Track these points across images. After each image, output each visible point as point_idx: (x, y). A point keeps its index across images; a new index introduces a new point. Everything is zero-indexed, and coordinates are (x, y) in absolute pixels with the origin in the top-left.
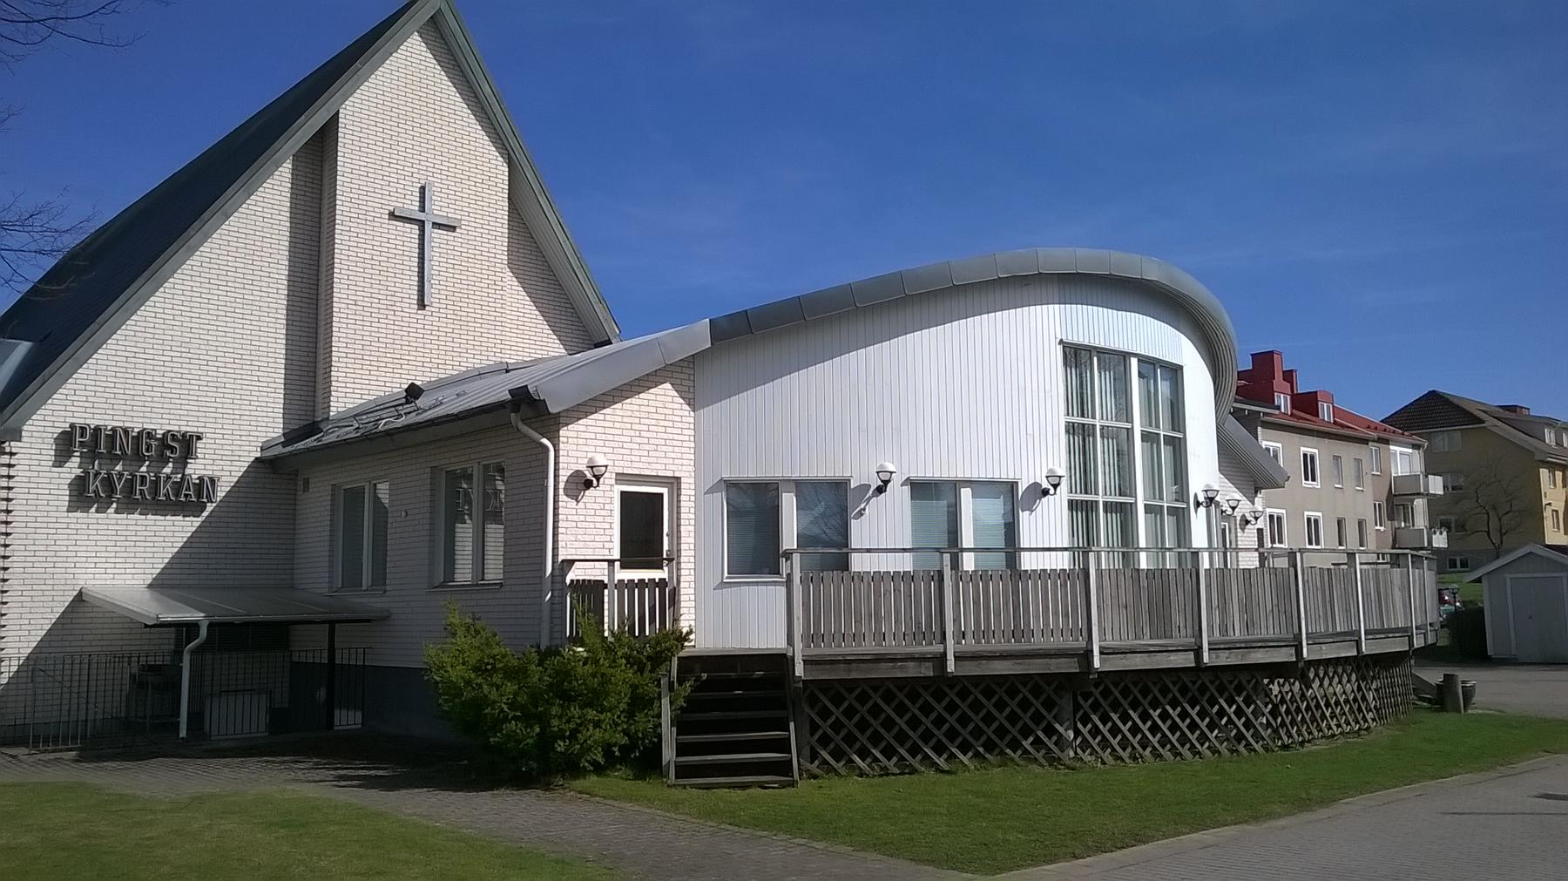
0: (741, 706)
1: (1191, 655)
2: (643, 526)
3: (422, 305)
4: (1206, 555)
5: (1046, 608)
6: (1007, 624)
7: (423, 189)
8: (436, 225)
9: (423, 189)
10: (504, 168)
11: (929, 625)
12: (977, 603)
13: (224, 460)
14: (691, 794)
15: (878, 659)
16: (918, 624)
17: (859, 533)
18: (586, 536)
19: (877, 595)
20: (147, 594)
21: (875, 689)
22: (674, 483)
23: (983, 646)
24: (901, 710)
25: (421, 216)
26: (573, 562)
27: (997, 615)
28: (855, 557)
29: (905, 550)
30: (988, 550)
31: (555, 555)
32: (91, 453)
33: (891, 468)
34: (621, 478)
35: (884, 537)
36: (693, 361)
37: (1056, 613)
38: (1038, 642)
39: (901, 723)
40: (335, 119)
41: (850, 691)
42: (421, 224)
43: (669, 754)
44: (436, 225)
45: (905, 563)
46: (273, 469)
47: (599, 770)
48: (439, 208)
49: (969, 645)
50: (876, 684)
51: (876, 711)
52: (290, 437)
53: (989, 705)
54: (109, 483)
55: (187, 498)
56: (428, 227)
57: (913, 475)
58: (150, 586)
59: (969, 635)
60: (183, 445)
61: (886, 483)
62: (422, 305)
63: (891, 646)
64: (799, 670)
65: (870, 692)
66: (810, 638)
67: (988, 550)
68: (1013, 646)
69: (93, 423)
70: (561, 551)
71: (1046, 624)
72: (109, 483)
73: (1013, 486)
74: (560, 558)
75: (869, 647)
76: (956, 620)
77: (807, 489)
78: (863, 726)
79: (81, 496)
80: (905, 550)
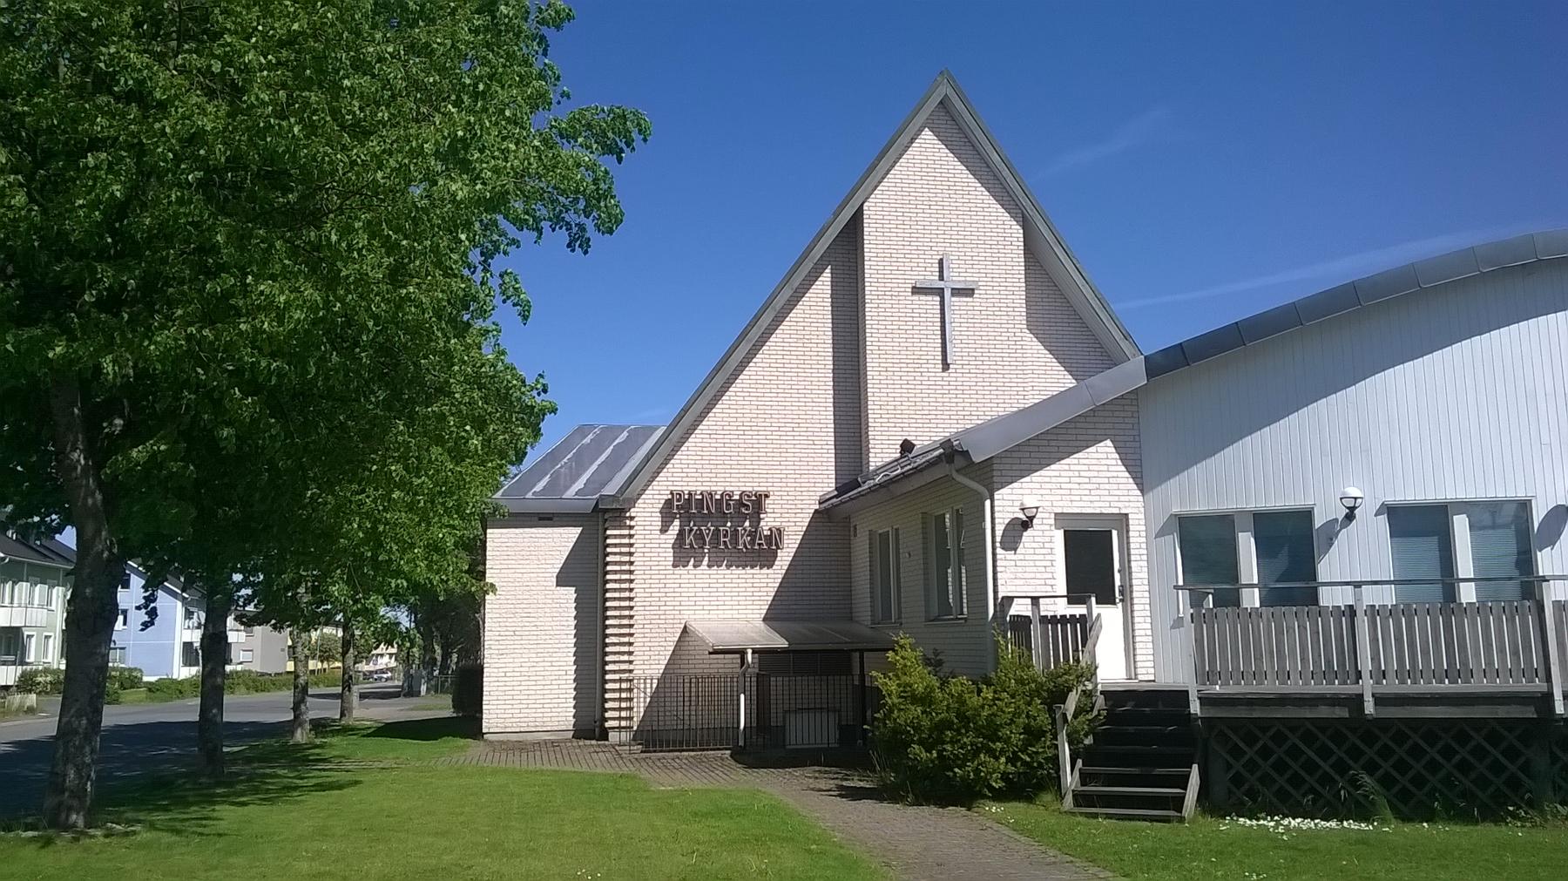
0: (1143, 744)
1: (287, 696)
2: (1091, 558)
3: (946, 366)
4: (36, 602)
5: (1488, 645)
6: (1316, 663)
7: (941, 262)
8: (957, 292)
9: (941, 262)
10: (1018, 232)
11: (1342, 663)
12: (1399, 640)
13: (790, 516)
14: (1102, 828)
15: (1283, 700)
16: (1329, 662)
17: (1326, 569)
18: (1030, 576)
19: (1279, 633)
20: (762, 625)
21: (1293, 730)
22: (1122, 520)
23: (1409, 687)
24: (1325, 753)
25: (941, 284)
26: (1012, 598)
27: (1425, 653)
28: (1323, 591)
29: (1556, 578)
30: (1409, 582)
31: (996, 592)
32: (686, 517)
33: (1354, 492)
34: (1060, 518)
35: (1358, 567)
36: (1133, 398)
37: (1502, 650)
38: (1481, 685)
39: (1512, 768)
40: (860, 210)
41: (1264, 730)
42: (940, 292)
43: (1070, 779)
44: (957, 292)
45: (1387, 597)
46: (830, 520)
47: (999, 796)
48: (957, 276)
49: (1391, 686)
50: (1293, 725)
51: (1295, 752)
52: (842, 489)
53: (1433, 753)
54: (700, 537)
55: (761, 552)
56: (947, 293)
57: (1391, 499)
58: (764, 620)
59: (1391, 675)
60: (754, 505)
61: (1352, 509)
62: (946, 366)
63: (1295, 686)
64: (1195, 707)
65: (1287, 732)
66: (1205, 676)
67: (1409, 582)
68: (1446, 686)
69: (686, 489)
70: (1000, 588)
71: (1490, 662)
72: (700, 537)
73: (1524, 506)
74: (1000, 595)
75: (1271, 687)
76: (1375, 658)
77: (1487, 514)
78: (1280, 767)
79: (684, 553)
80: (1556, 578)
